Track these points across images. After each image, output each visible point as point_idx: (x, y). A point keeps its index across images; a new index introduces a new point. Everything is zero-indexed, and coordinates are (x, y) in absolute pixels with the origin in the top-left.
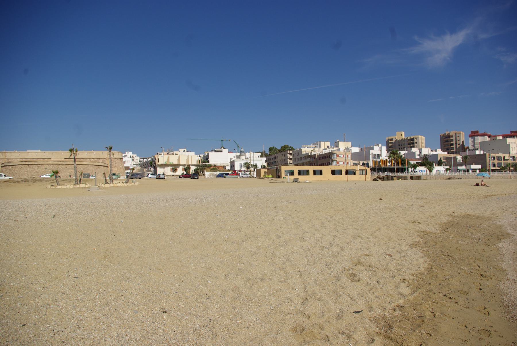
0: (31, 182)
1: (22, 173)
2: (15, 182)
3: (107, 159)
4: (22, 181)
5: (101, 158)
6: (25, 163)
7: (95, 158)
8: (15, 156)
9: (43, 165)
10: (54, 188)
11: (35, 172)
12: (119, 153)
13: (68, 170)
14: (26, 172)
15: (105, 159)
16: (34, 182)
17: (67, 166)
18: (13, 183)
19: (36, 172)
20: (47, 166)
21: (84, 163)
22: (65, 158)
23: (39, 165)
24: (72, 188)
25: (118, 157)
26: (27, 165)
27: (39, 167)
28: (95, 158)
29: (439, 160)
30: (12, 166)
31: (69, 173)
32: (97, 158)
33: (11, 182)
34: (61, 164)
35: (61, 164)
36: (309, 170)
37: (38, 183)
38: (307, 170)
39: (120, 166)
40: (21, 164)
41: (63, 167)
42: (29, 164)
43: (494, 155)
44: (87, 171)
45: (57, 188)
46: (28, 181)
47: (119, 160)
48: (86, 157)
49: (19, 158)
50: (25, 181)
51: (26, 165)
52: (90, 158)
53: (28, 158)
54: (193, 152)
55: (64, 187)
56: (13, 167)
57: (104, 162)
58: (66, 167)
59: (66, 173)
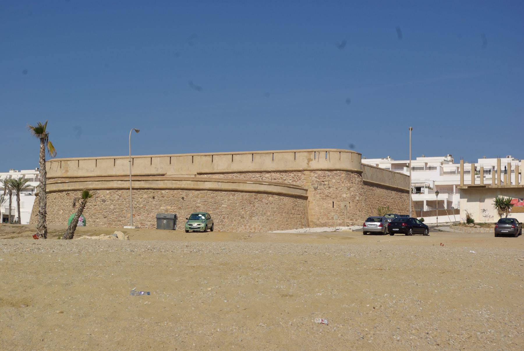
3: (305, 172)
5: (246, 170)
7: (274, 172)
12: (343, 155)
13: (157, 207)
15: (300, 174)
21: (208, 185)
22: (199, 171)
25: (338, 167)
28: (274, 172)
32: (323, 170)
34: (140, 189)
36: (495, 236)
39: (344, 196)
41: (145, 196)
42: (70, 188)
43: (131, 156)
48: (251, 169)
51: (64, 193)
52: (261, 172)
58: (154, 198)
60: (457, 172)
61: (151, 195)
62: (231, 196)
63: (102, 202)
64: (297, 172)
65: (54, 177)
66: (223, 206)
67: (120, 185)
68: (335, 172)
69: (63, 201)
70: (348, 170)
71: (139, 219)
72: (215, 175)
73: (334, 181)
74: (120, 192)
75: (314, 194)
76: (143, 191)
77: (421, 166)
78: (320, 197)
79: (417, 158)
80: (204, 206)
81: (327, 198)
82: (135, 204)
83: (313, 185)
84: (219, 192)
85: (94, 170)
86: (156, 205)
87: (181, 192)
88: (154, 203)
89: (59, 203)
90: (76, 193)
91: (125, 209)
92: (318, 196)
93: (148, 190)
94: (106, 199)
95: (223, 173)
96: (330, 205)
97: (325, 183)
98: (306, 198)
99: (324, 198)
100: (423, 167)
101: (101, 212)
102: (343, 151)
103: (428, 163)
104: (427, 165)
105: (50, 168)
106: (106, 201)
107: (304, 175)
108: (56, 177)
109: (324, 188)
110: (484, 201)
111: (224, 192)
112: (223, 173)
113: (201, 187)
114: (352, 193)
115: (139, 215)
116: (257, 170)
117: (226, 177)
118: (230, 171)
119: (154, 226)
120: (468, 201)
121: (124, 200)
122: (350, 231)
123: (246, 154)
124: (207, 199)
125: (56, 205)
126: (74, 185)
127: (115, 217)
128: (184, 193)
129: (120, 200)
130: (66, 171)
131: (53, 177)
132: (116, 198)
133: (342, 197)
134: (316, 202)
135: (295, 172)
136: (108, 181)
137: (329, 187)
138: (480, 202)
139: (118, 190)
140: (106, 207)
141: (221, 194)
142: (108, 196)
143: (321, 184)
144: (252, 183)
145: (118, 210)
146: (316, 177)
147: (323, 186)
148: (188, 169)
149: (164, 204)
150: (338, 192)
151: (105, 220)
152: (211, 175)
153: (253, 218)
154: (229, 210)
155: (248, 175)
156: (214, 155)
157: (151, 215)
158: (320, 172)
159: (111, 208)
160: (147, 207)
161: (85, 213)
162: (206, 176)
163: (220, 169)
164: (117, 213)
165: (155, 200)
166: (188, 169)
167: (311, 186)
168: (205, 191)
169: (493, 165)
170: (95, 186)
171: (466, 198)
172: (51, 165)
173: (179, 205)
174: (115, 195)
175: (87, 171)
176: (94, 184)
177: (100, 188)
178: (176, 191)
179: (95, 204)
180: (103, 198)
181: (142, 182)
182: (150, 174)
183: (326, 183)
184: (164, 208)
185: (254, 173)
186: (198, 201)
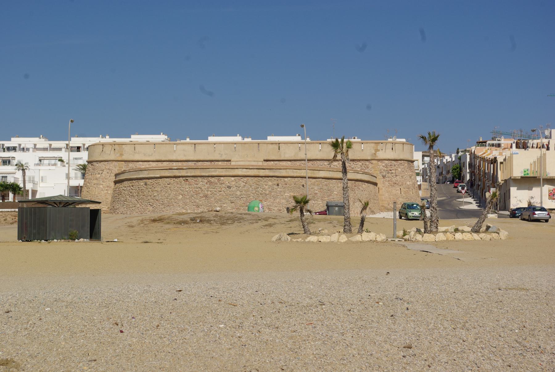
0: (215, 224)
1: (171, 199)
2: (177, 223)
3: (373, 161)
4: (193, 220)
5: (314, 158)
6: (177, 173)
8: (145, 155)
9: (222, 178)
10: (302, 242)
11: (201, 197)
13: (282, 193)
14: (181, 196)
15: (367, 163)
16: (222, 224)
17: (279, 182)
18: (175, 226)
19: (206, 196)
20: (232, 181)
22: (266, 159)
23: (212, 180)
24: (345, 242)
25: (402, 157)
26: (183, 177)
27: (211, 183)
29: (467, 180)
30: (144, 181)
31: (284, 201)
32: (389, 160)
33: (168, 223)
34: (265, 177)
35: (265, 177)
37: (231, 226)
38: (505, 211)
39: (408, 183)
40: (169, 175)
41: (270, 183)
42: (189, 174)
44: (329, 196)
45: (307, 240)
46: (209, 221)
47: (406, 164)
48: (319, 158)
49: (154, 159)
50: (201, 221)
51: (181, 178)
53: (174, 158)
54: (208, 138)
55: (324, 239)
56: (148, 183)
57: (366, 171)
58: (278, 185)
59: (277, 201)
60: (50, 149)
61: (276, 182)
62: (339, 184)
63: (227, 188)
64: (364, 161)
65: (108, 160)
66: (335, 192)
67: (245, 172)
68: (400, 162)
69: (181, 187)
70: (409, 160)
71: (266, 205)
72: (282, 162)
73: (399, 170)
74: (245, 179)
75: (383, 181)
76: (268, 178)
77: (46, 147)
78: (389, 184)
79: (12, 139)
80: (320, 193)
81: (395, 185)
82: (261, 191)
83: (381, 174)
84: (331, 180)
85: (152, 154)
86: (281, 192)
87: (301, 180)
88: (279, 190)
89: (175, 188)
90: (197, 179)
91: (251, 195)
92: (387, 183)
93: (272, 178)
94: (231, 186)
95: (290, 161)
96: (398, 192)
97: (392, 171)
98: (375, 184)
99: (393, 185)
100: (47, 147)
101: (227, 197)
102: (384, 142)
103: (52, 144)
104: (51, 147)
105: (103, 151)
106: (232, 187)
107: (372, 164)
108: (110, 160)
109: (391, 176)
110: (532, 190)
111: (334, 180)
112: (290, 161)
113: (318, 176)
114: (413, 181)
115: (266, 200)
116: (325, 159)
117: (293, 164)
118: (299, 158)
119: (281, 211)
120: (517, 189)
121: (250, 187)
122: (496, 217)
123: (314, 143)
124: (322, 187)
125: (171, 190)
126: (193, 172)
127: (243, 202)
128: (303, 181)
129: (246, 187)
130: (120, 155)
131: (106, 160)
132: (242, 185)
133: (407, 185)
134: (385, 189)
135: (362, 161)
136: (233, 169)
137: (396, 176)
138: (529, 190)
139: (243, 178)
140: (233, 193)
141: (332, 182)
142: (234, 183)
143: (388, 173)
144: (353, 172)
145: (245, 196)
146: (383, 166)
147: (391, 174)
148: (254, 156)
149: (288, 191)
150: (404, 180)
151: (233, 205)
152: (278, 162)
153: (355, 204)
154: (338, 196)
155: (316, 162)
156: (281, 143)
157: (277, 201)
158: (387, 162)
159: (237, 194)
160: (272, 194)
161: (210, 199)
162: (272, 162)
163: (287, 157)
164: (245, 199)
165: (279, 187)
166: (254, 156)
167: (379, 174)
168: (320, 179)
169: (35, 143)
170: (219, 173)
171: (516, 187)
172: (103, 148)
173: (301, 192)
174: (241, 182)
175: (144, 155)
176: (218, 172)
177: (225, 175)
178: (296, 179)
179: (220, 190)
180: (228, 184)
181: (267, 170)
182: (214, 160)
183: (393, 171)
184: (288, 195)
185: (322, 161)
186: (316, 188)
